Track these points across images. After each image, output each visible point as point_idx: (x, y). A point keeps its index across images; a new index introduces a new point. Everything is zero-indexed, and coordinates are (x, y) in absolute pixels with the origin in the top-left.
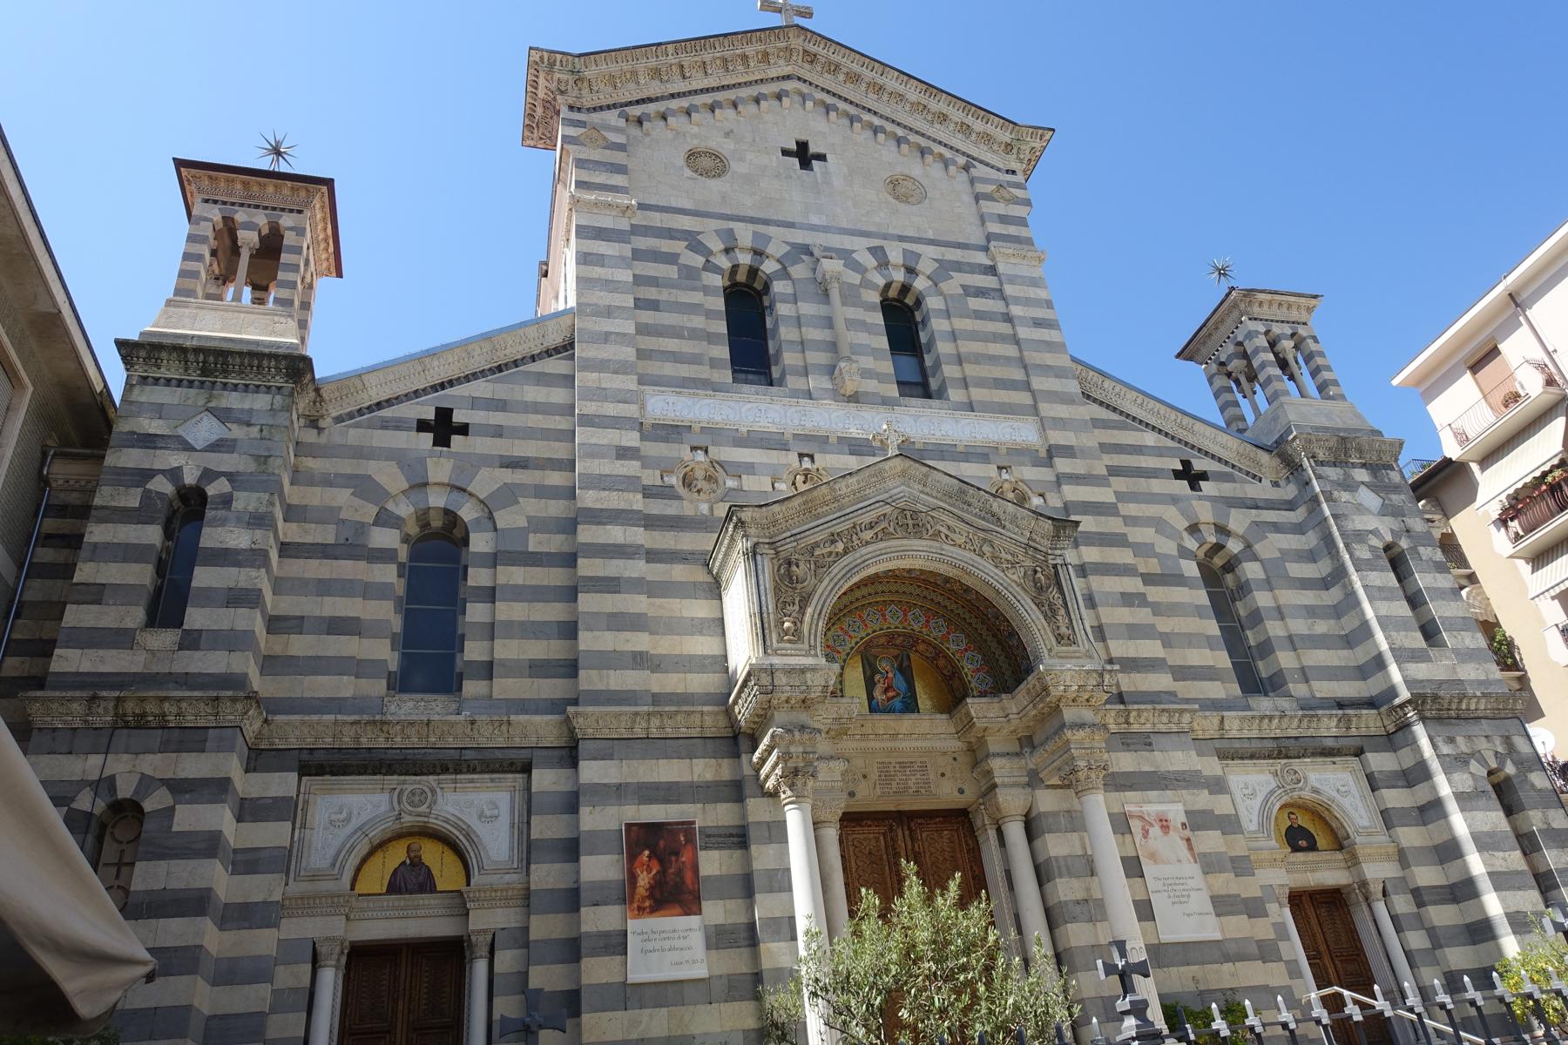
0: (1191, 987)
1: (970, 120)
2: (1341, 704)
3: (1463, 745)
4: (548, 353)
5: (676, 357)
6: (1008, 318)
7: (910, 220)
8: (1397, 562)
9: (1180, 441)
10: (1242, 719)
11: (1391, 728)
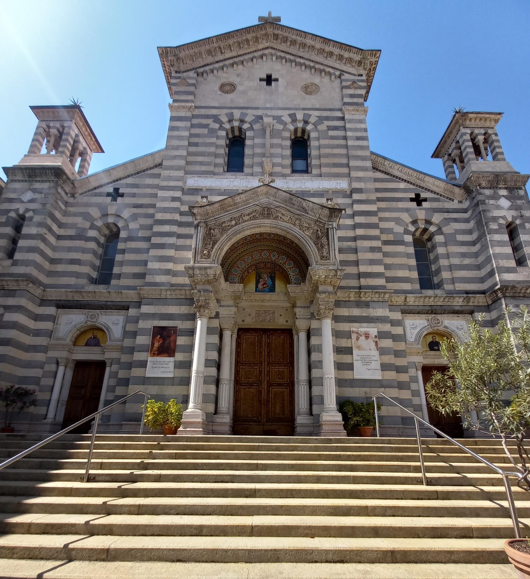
0: (363, 395)
1: (342, 53)
2: (467, 292)
4: (156, 166)
5: (201, 163)
7: (311, 101)
9: (417, 186)
10: (415, 297)
11: (490, 303)
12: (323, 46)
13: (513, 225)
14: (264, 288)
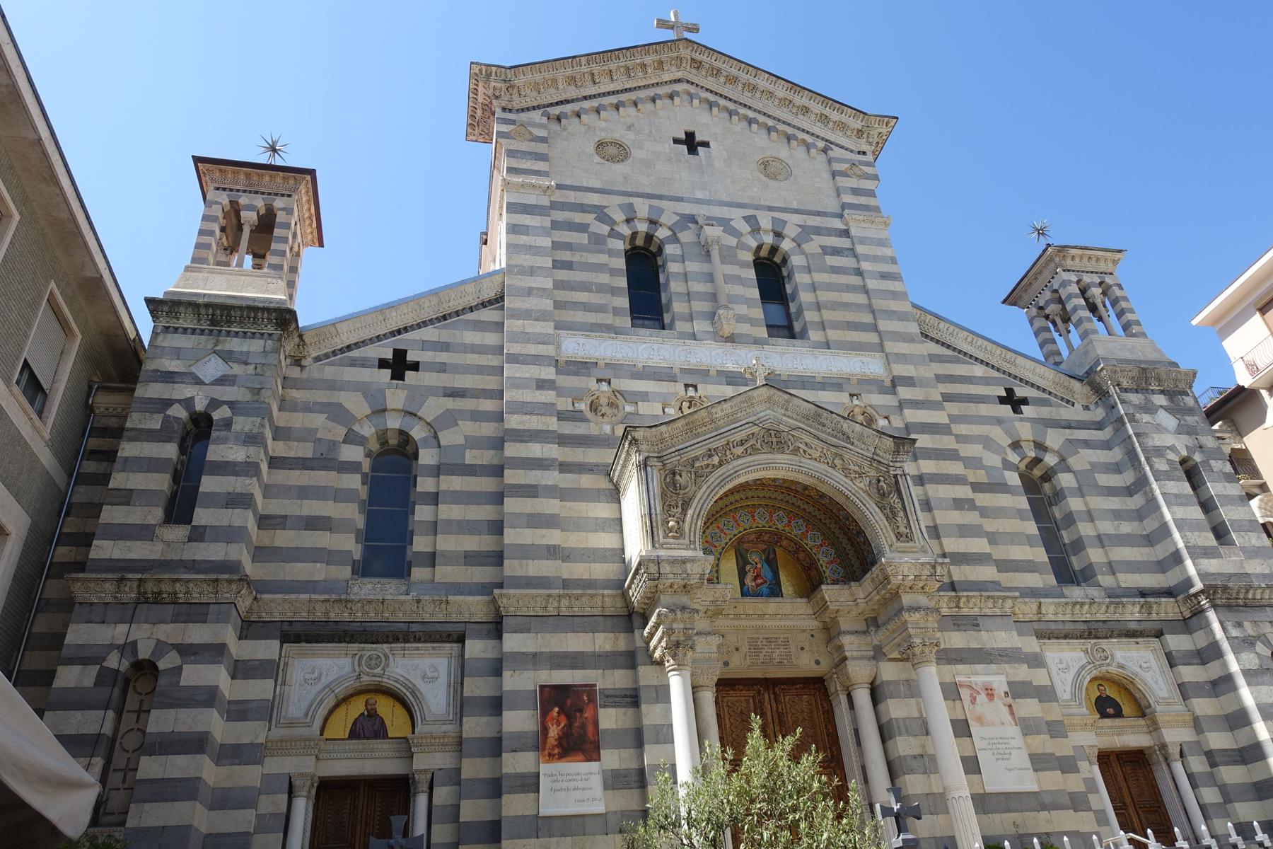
1: (827, 111)
2: (1143, 593)
3: (1249, 629)
4: (484, 305)
5: (586, 307)
6: (859, 272)
7: (778, 193)
8: (1192, 474)
9: (1004, 372)
12: (789, 95)
13: (1190, 463)
14: (758, 586)
